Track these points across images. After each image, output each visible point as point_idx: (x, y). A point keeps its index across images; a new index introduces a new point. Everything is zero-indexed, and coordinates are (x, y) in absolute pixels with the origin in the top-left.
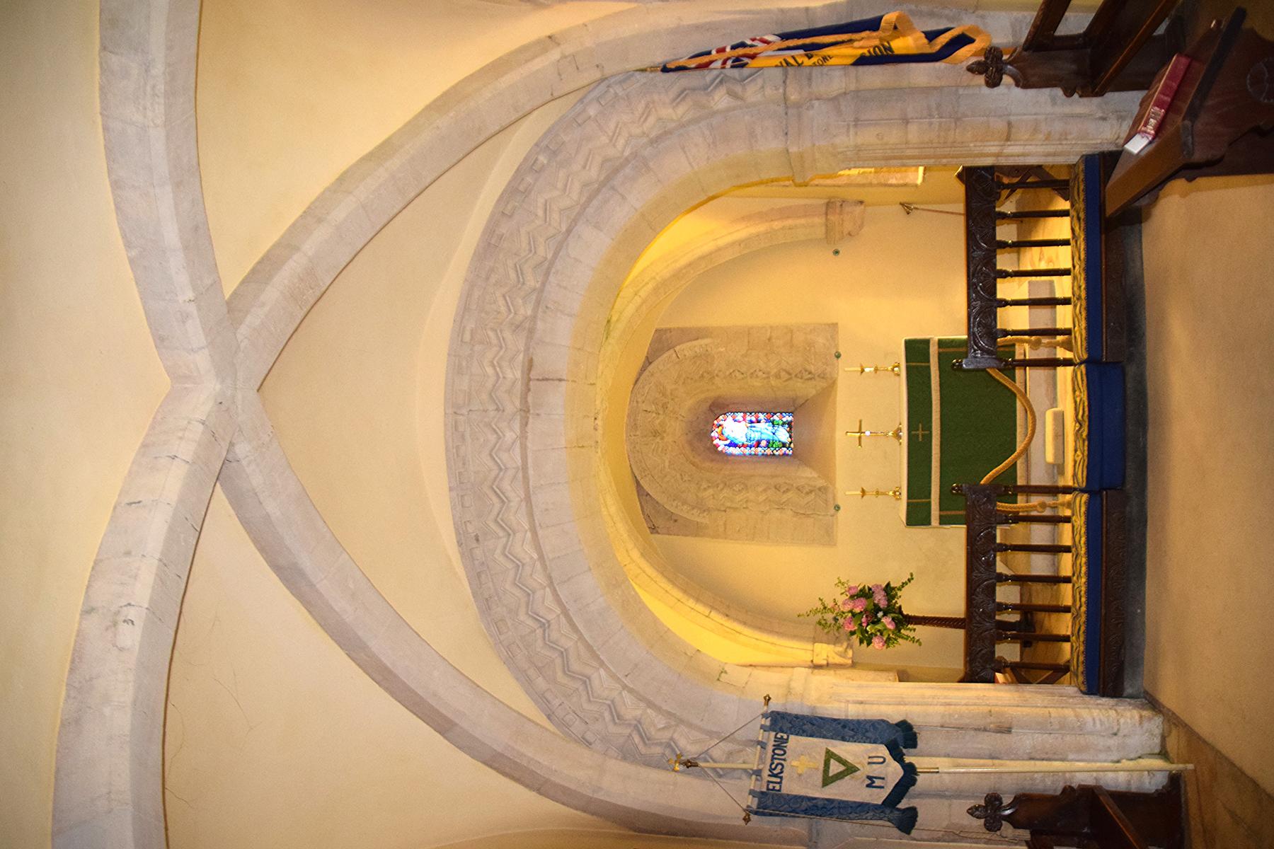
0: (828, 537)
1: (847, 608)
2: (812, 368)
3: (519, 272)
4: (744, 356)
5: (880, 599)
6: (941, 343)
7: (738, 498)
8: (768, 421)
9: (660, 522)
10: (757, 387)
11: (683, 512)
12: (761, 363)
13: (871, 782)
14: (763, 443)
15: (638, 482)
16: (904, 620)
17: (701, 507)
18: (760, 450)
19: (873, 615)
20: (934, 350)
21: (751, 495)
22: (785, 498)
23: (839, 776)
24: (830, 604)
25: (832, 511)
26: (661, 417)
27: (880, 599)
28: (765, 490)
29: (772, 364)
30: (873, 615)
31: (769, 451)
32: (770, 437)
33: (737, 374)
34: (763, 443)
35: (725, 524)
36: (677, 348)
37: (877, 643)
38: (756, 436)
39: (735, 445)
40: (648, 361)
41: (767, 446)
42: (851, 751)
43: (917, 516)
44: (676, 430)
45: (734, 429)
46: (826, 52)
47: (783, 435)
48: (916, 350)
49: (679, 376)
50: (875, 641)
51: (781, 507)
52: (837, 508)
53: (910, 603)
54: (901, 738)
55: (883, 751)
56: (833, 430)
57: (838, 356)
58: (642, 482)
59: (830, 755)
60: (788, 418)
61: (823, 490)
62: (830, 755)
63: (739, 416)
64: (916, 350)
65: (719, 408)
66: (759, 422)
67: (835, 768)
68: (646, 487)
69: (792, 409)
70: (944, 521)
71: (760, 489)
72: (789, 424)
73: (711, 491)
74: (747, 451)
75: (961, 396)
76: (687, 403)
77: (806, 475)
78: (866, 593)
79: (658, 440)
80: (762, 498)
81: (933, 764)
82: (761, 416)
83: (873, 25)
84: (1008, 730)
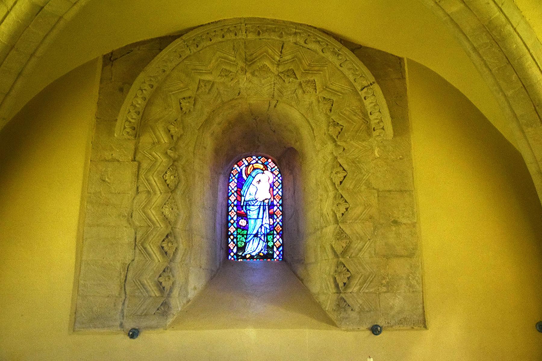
2: (354, 288)
4: (369, 185)
7: (155, 180)
8: (272, 227)
11: (135, 98)
12: (359, 210)
14: (243, 222)
18: (233, 214)
22: (153, 250)
25: (130, 325)
26: (274, 69)
28: (165, 219)
29: (358, 227)
31: (232, 229)
32: (252, 231)
33: (341, 175)
34: (243, 222)
35: (113, 160)
36: (376, 87)
38: (253, 214)
39: (240, 185)
40: (356, 49)
41: (239, 227)
44: (256, 90)
45: (261, 185)
47: (254, 247)
49: (335, 92)
51: (139, 244)
52: (134, 334)
56: (259, 324)
57: (375, 330)
58: (179, 41)
61: (164, 309)
66: (271, 216)
69: (288, 258)
71: (167, 211)
72: (272, 256)
73: (165, 139)
77: (191, 279)
79: (241, 64)
80: (154, 214)
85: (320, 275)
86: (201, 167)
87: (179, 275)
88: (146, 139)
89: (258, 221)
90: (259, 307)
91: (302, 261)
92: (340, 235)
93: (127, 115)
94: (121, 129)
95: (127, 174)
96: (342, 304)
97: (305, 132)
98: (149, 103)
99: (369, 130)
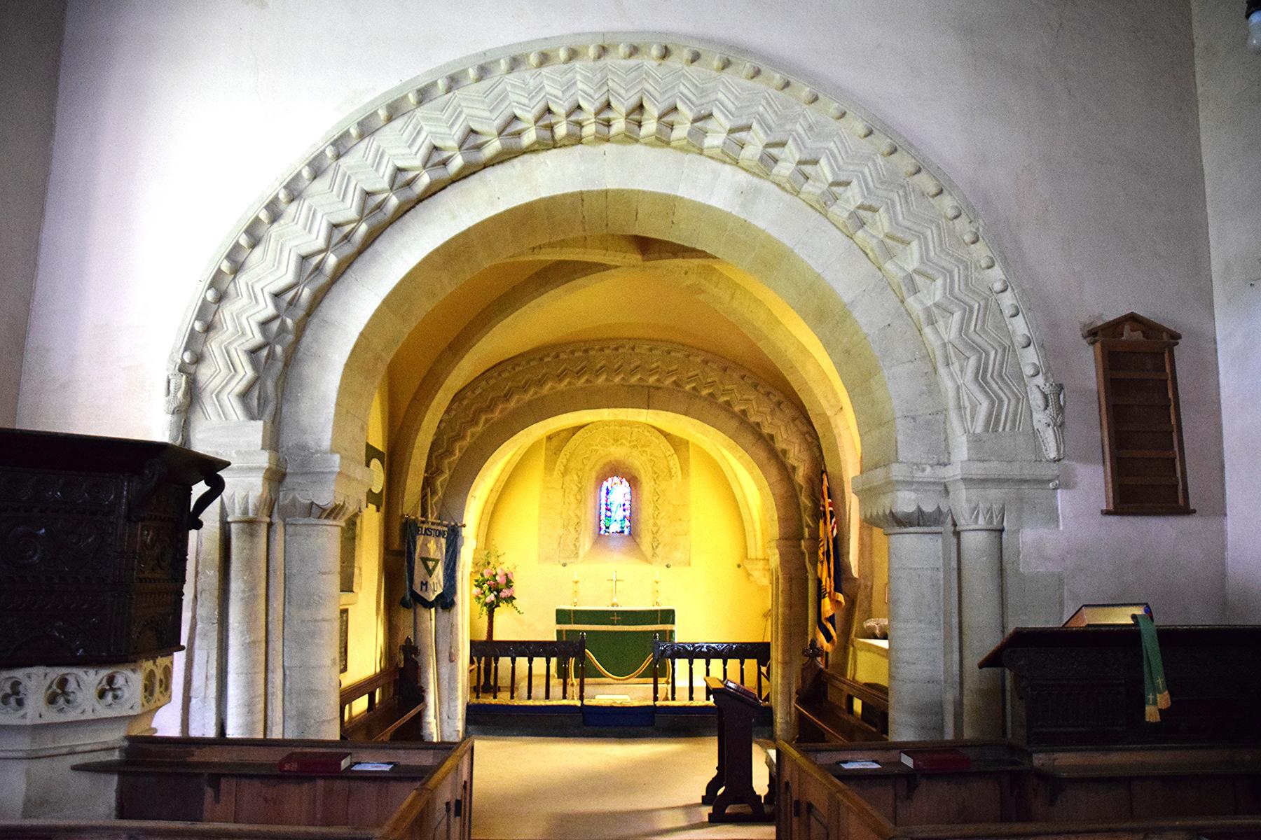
0: (545, 558)
1: (499, 571)
2: (660, 547)
3: (712, 384)
5: (504, 594)
6: (672, 632)
7: (572, 498)
9: (555, 442)
10: (647, 512)
11: (562, 458)
13: (425, 584)
15: (582, 427)
16: (491, 608)
17: (565, 472)
19: (495, 589)
20: (668, 627)
21: (573, 506)
22: (572, 529)
23: (427, 567)
24: (501, 559)
27: (504, 594)
30: (495, 589)
31: (603, 517)
37: (476, 590)
42: (439, 572)
43: (562, 616)
44: (618, 452)
46: (825, 563)
47: (615, 527)
48: (668, 616)
50: (478, 589)
51: (566, 527)
52: (564, 565)
53: (501, 613)
54: (446, 602)
55: (440, 591)
59: (437, 561)
60: (627, 531)
62: (437, 561)
63: (628, 497)
64: (668, 616)
65: (633, 482)
67: (431, 564)
68: (578, 434)
70: (559, 632)
72: (622, 532)
73: (575, 478)
74: (603, 502)
75: (642, 640)
76: (638, 462)
77: (586, 543)
78: (509, 583)
81: (430, 618)
82: (627, 513)
83: (838, 588)
84: (451, 661)
85: (646, 540)
86: (590, 485)
87: (581, 539)
88: (567, 478)
89: (618, 514)
90: (617, 556)
91: (638, 536)
92: (655, 524)
93: (559, 467)
94: (556, 474)
95: (560, 493)
96: (654, 555)
97: (642, 472)
98: (568, 461)
99: (671, 476)
